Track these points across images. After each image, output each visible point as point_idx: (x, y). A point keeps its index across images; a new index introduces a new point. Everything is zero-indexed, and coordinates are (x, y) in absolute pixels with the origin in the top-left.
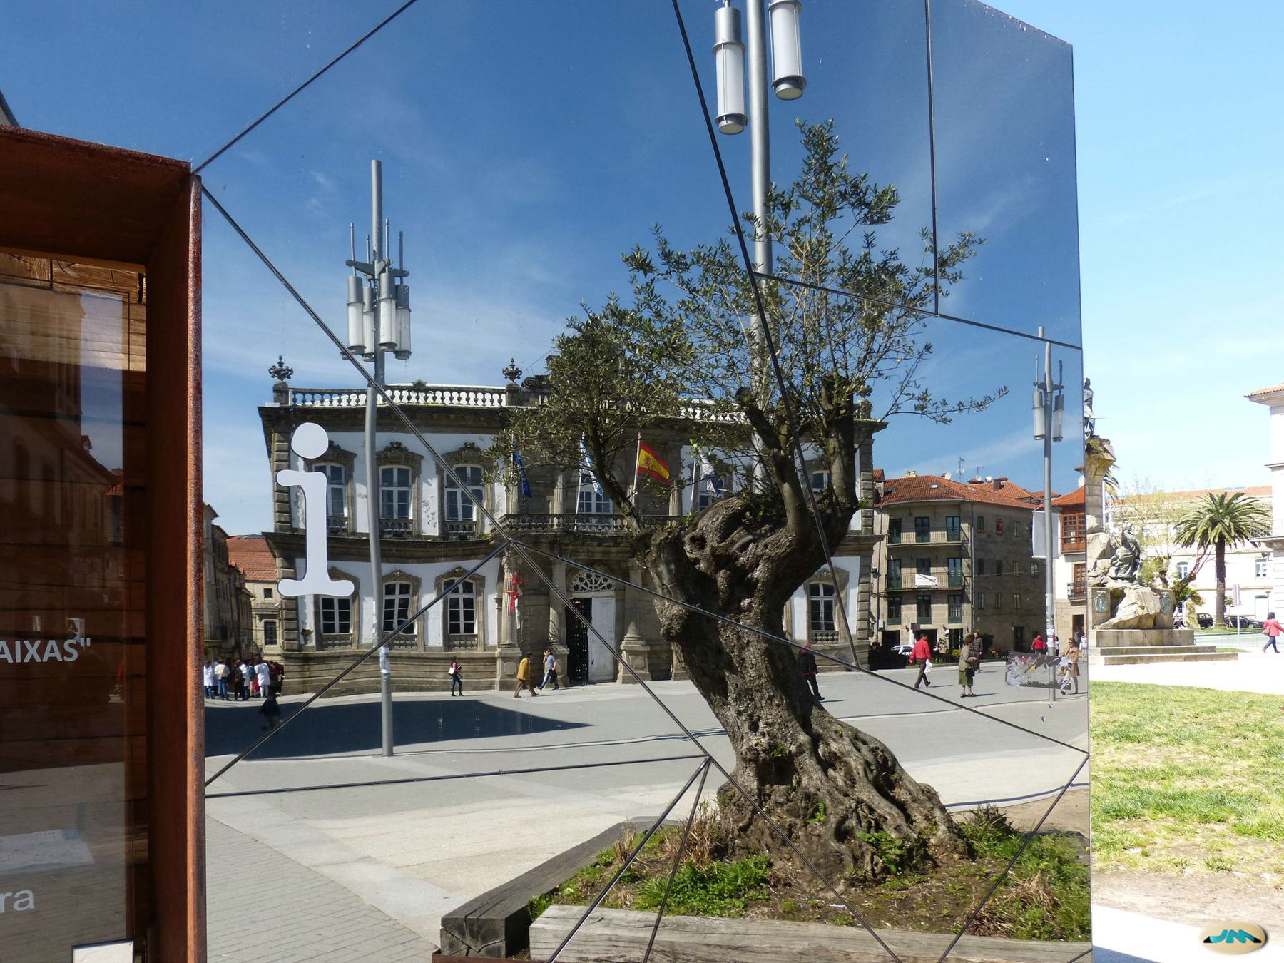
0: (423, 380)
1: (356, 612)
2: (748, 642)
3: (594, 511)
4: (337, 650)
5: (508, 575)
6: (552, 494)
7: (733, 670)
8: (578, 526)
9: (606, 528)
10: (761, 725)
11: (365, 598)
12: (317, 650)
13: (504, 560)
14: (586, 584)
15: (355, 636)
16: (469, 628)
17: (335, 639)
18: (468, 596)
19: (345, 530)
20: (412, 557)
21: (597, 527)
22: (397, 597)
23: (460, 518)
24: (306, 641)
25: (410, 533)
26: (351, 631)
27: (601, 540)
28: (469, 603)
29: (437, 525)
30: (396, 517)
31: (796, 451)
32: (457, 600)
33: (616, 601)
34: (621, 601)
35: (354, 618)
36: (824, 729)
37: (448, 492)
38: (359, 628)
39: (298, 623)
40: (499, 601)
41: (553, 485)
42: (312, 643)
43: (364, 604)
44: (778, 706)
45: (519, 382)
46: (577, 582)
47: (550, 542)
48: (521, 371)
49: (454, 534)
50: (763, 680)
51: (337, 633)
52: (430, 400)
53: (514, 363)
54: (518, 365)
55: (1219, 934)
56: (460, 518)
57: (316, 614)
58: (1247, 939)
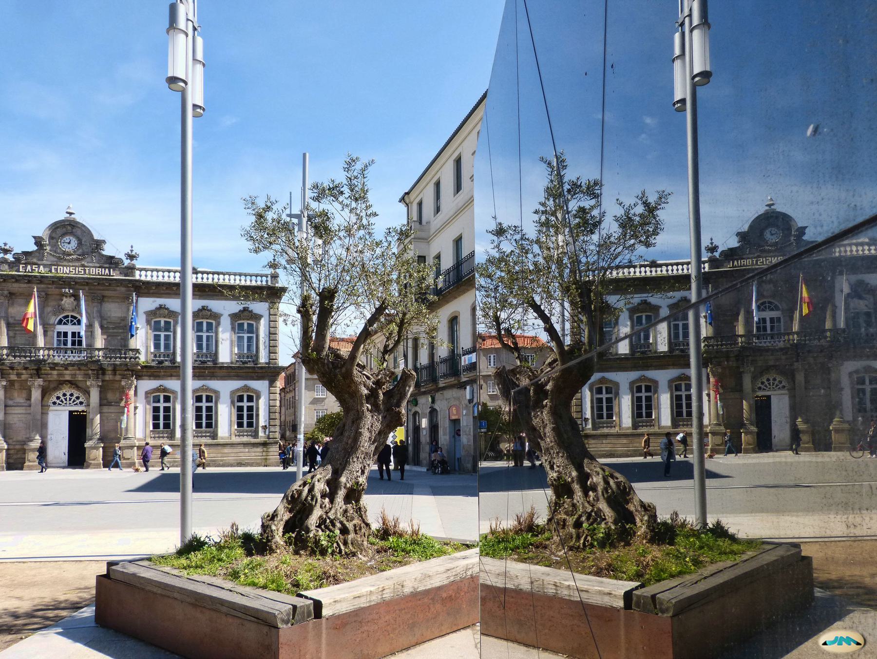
0: (655, 259)
1: (617, 405)
2: (546, 424)
3: (769, 331)
4: (606, 431)
5: (712, 380)
6: (737, 320)
7: (542, 439)
8: (756, 343)
9: (777, 342)
10: (555, 467)
11: (624, 396)
12: (593, 430)
13: (709, 370)
14: (766, 386)
15: (618, 422)
16: (649, 415)
17: (604, 423)
18: (648, 394)
19: (611, 353)
20: (651, 366)
21: (770, 342)
22: (604, 396)
23: (681, 339)
24: (586, 425)
25: (650, 351)
26: (614, 418)
27: (773, 351)
28: (649, 399)
29: (667, 345)
30: (642, 342)
31: (568, 341)
32: (681, 396)
33: (789, 397)
34: (792, 397)
35: (616, 409)
36: (591, 470)
37: (674, 324)
38: (620, 417)
39: (582, 414)
40: (708, 395)
41: (738, 314)
42: (590, 426)
43: (622, 400)
44: (562, 457)
45: (717, 254)
46: (760, 385)
47: (736, 356)
48: (718, 247)
49: (677, 349)
50: (553, 444)
51: (605, 419)
52: (659, 272)
53: (713, 241)
54: (716, 243)
55: (833, 639)
56: (681, 339)
57: (592, 408)
58: (852, 643)
